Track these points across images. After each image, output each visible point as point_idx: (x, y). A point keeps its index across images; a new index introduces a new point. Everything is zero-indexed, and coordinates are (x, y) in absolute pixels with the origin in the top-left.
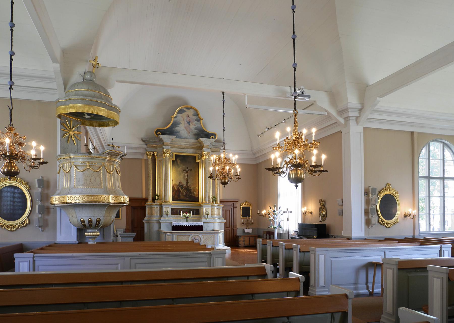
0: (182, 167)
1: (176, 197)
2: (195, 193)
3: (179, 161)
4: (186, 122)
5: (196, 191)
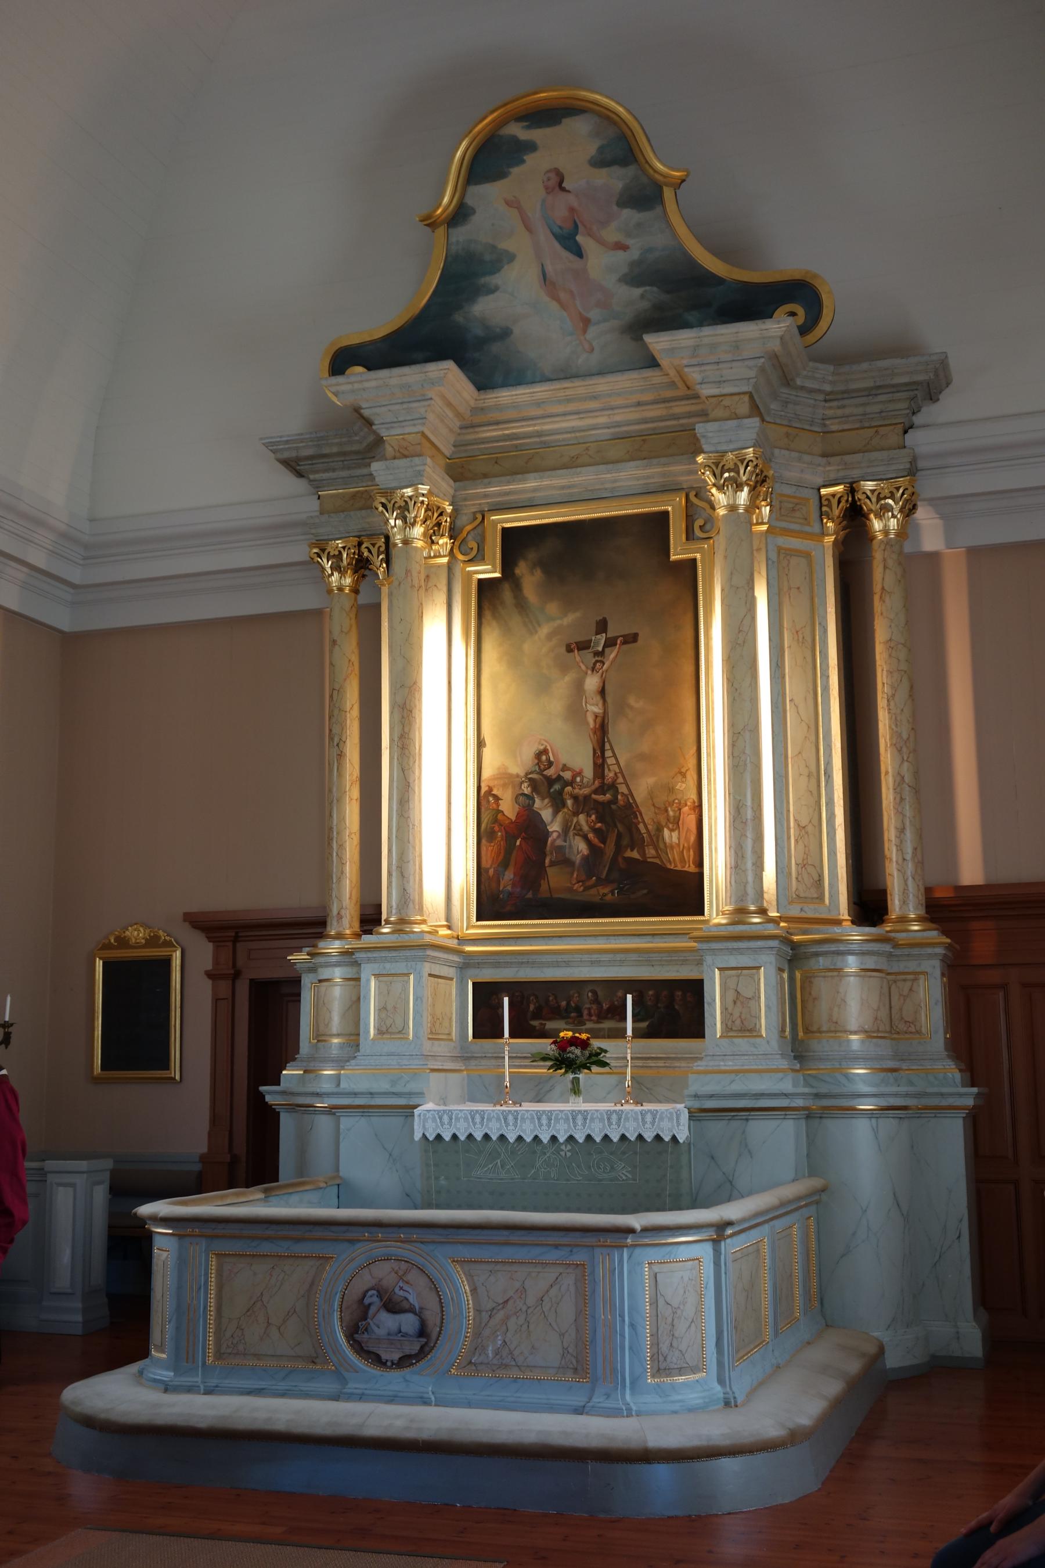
0: (556, 620)
2: (670, 836)
3: (530, 578)
4: (544, 236)
5: (676, 823)
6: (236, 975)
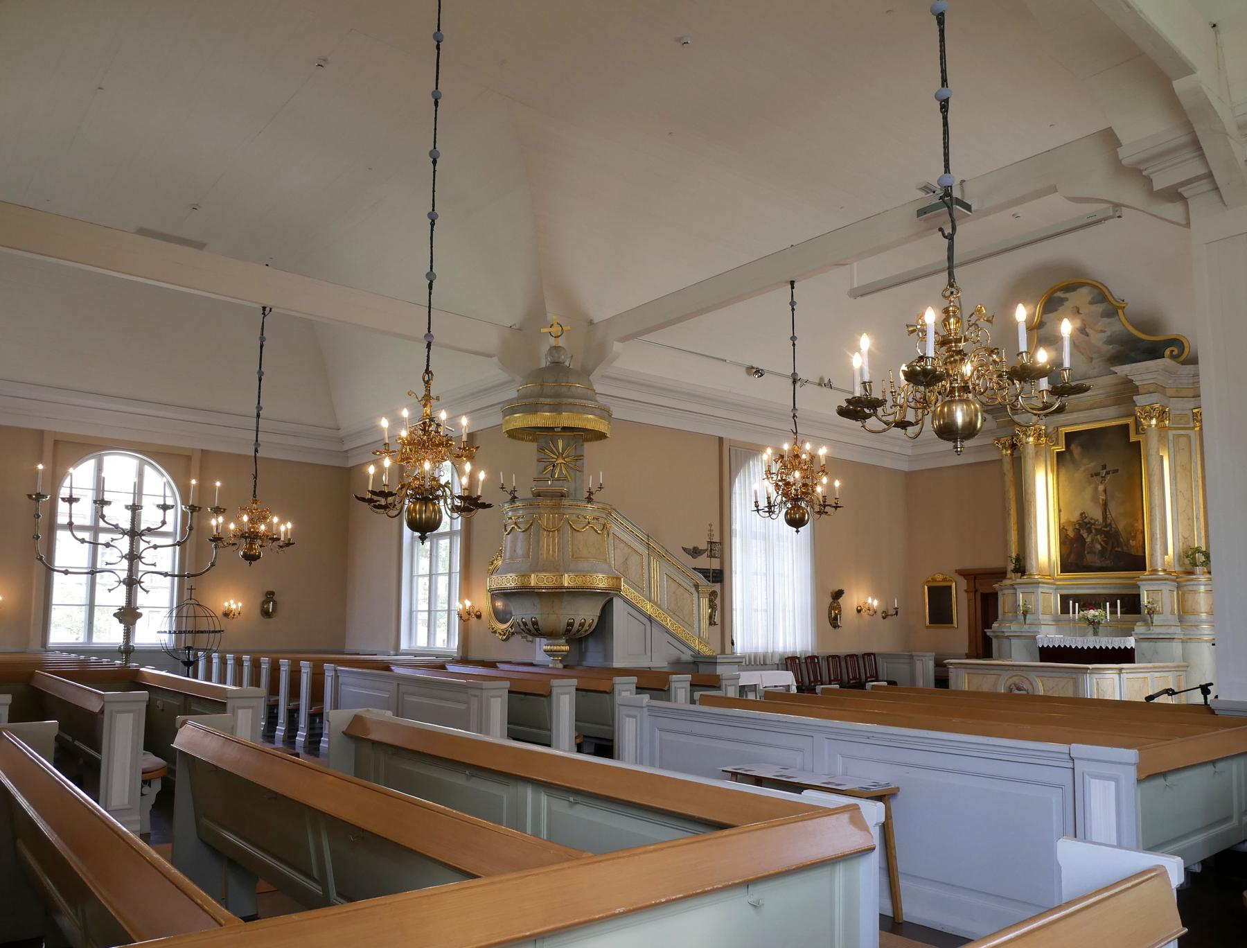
0: (1091, 465)
1: (1072, 558)
2: (1132, 543)
5: (1134, 538)
6: (976, 591)
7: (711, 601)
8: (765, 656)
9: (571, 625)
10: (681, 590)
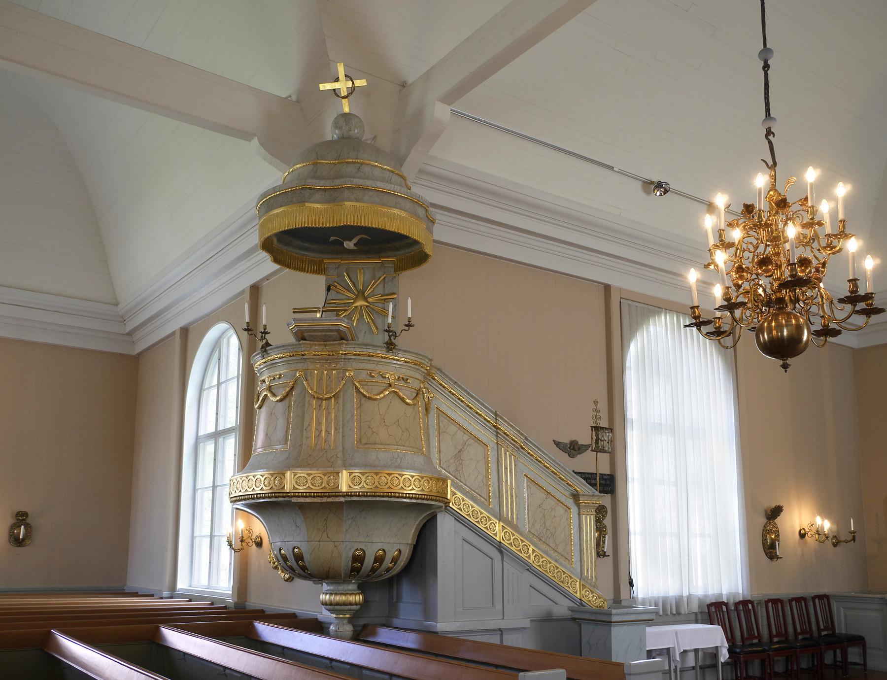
7: (598, 521)
8: (679, 601)
9: (358, 559)
10: (551, 502)
